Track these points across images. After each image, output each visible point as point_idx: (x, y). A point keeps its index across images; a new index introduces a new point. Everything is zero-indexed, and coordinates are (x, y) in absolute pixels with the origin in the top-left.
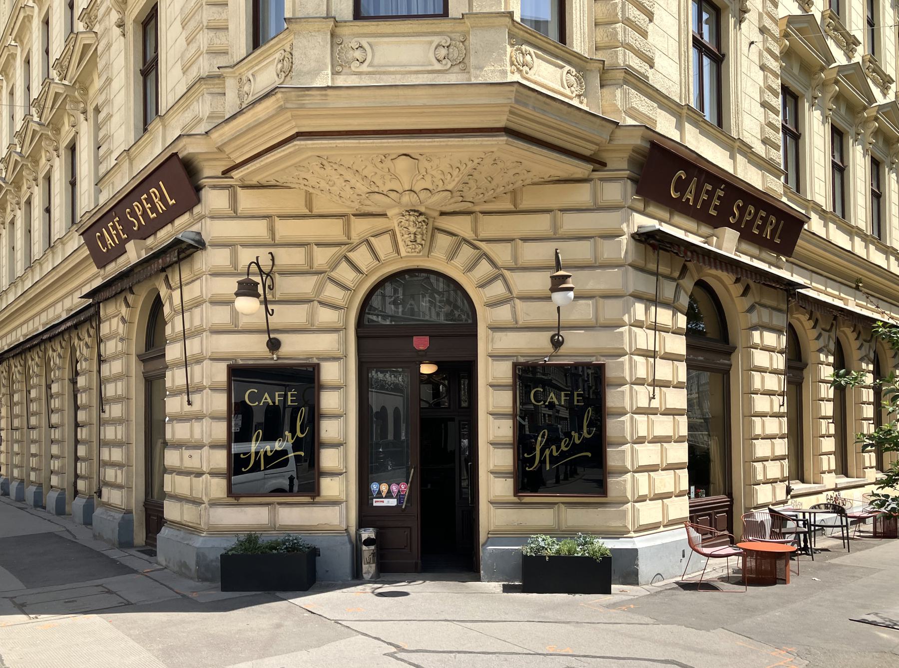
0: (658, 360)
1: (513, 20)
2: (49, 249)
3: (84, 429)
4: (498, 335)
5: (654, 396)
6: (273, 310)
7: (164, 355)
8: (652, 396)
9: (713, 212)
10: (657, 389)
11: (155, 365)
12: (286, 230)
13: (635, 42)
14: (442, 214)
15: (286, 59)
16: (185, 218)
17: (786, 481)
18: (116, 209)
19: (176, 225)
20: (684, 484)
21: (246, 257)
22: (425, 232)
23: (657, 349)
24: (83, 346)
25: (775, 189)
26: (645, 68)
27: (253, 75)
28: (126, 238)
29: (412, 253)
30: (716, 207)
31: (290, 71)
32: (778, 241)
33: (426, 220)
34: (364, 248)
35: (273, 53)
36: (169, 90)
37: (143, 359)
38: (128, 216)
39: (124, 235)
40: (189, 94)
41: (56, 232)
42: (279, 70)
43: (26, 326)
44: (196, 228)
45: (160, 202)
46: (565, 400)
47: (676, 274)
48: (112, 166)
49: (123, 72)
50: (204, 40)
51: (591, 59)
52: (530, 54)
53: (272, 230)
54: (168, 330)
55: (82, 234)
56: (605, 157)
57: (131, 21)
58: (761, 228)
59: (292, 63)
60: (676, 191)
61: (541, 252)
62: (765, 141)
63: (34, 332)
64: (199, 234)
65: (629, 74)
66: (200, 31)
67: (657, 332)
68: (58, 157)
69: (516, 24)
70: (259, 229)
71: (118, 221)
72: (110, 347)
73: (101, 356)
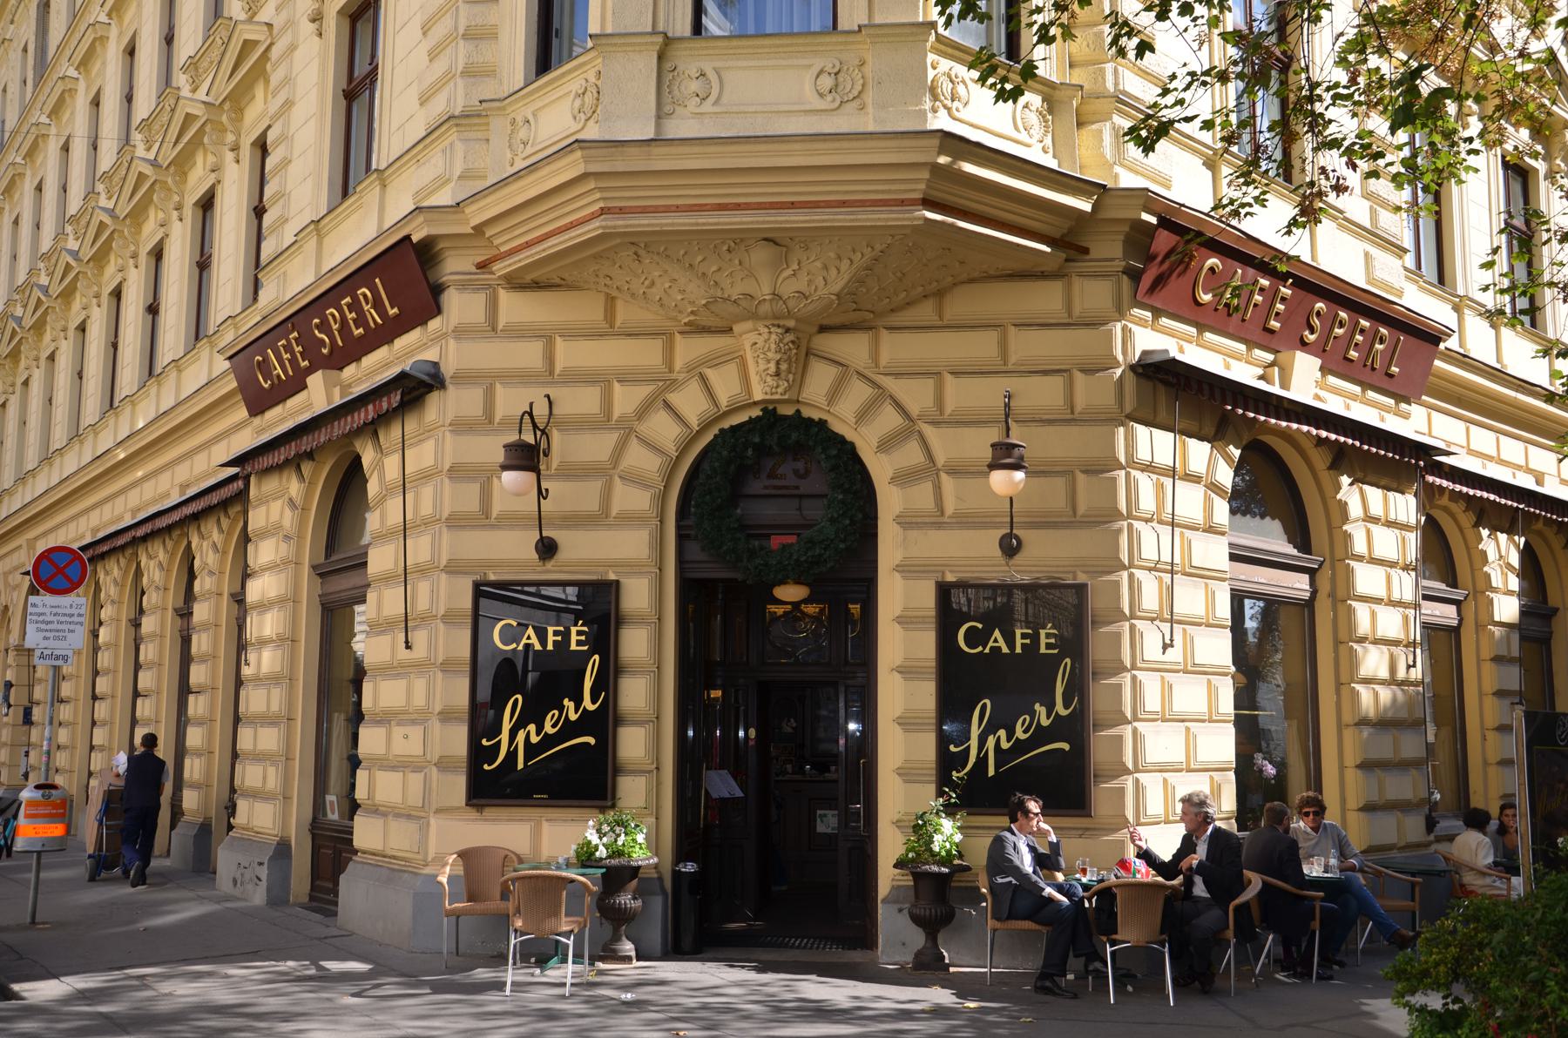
4: (913, 534)
6: (547, 490)
7: (365, 563)
8: (1168, 641)
12: (569, 354)
14: (823, 329)
15: (588, 93)
16: (413, 337)
18: (293, 320)
19: (395, 348)
21: (511, 403)
23: (1177, 560)
24: (208, 547)
27: (534, 115)
28: (308, 368)
29: (772, 394)
31: (594, 112)
34: (694, 387)
35: (570, 79)
36: (393, 128)
37: (323, 573)
38: (316, 332)
41: (166, 349)
42: (576, 111)
44: (431, 355)
45: (372, 311)
48: (284, 247)
49: (315, 90)
50: (461, 53)
52: (964, 82)
53: (550, 358)
54: (373, 521)
55: (230, 358)
57: (334, 14)
59: (598, 100)
61: (985, 394)
63: (113, 523)
64: (436, 365)
66: (450, 43)
68: (181, 220)
70: (529, 355)
71: (296, 339)
72: (264, 553)
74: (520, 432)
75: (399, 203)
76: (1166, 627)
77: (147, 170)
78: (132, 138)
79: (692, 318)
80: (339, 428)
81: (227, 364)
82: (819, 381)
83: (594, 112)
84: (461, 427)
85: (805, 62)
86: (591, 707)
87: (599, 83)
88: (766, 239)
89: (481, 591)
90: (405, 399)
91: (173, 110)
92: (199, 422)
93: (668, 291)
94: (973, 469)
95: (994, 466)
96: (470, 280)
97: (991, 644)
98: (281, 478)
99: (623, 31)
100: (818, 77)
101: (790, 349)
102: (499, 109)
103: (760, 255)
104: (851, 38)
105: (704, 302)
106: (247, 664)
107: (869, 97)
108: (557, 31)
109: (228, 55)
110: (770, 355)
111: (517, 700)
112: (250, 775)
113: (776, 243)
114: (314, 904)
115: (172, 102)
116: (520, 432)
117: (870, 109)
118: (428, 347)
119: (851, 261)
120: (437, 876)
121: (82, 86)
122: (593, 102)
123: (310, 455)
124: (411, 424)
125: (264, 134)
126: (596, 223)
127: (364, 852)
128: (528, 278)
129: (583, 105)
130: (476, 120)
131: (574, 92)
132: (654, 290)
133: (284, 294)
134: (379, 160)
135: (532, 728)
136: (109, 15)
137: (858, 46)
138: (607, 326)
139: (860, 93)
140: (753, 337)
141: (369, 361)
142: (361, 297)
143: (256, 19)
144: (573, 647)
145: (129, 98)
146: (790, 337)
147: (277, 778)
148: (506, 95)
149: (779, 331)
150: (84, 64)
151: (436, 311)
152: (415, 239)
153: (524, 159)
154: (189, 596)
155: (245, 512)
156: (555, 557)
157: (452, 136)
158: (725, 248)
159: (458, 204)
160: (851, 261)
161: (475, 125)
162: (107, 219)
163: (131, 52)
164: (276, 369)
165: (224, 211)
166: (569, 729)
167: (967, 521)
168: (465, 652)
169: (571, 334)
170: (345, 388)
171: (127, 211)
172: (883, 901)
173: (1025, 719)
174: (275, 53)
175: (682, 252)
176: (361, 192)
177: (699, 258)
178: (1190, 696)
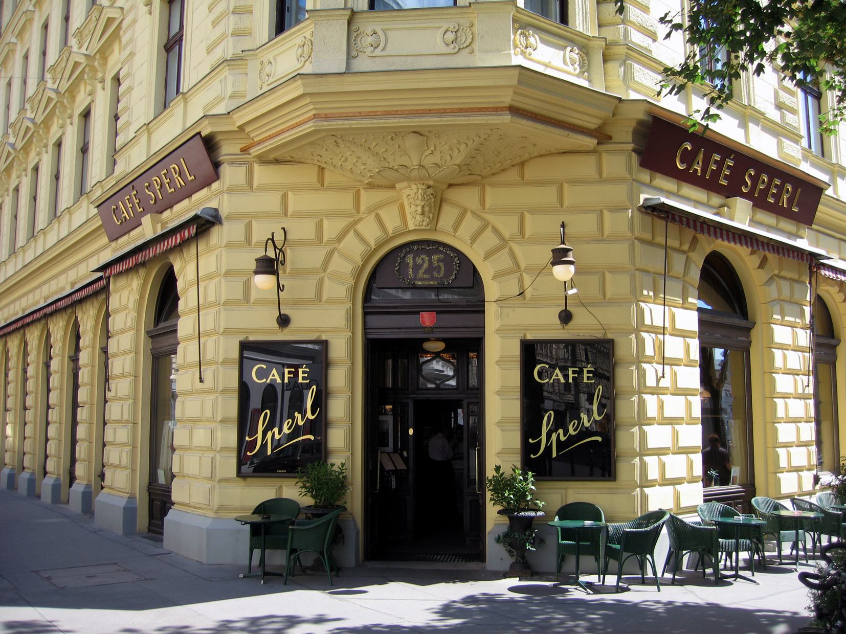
0: (667, 337)
1: (517, 7)
2: (56, 219)
3: (54, 411)
5: (663, 374)
6: (283, 286)
7: (176, 330)
9: (724, 183)
10: (667, 368)
11: (165, 342)
13: (636, 19)
14: (450, 186)
16: (204, 192)
17: (813, 470)
20: (698, 470)
21: (261, 232)
22: (433, 205)
24: (88, 318)
25: (792, 155)
26: (648, 42)
27: (274, 59)
30: (726, 177)
31: (309, 57)
33: (435, 194)
35: (296, 36)
37: (152, 336)
40: (212, 74)
43: (25, 298)
44: (214, 204)
45: (179, 178)
46: (573, 378)
47: (686, 247)
50: (231, 23)
51: (593, 37)
55: (98, 207)
56: (610, 130)
58: (778, 197)
59: (312, 49)
60: (682, 162)
62: (780, 106)
64: (216, 210)
65: (631, 50)
66: (226, 16)
67: (666, 308)
68: (72, 124)
69: (520, 10)
73: (109, 332)
74: (266, 251)
75: (195, 114)
76: (660, 368)
77: (53, 95)
78: (45, 77)
79: (370, 180)
80: (160, 248)
81: (96, 211)
82: (448, 216)
83: (309, 57)
84: (230, 246)
85: (437, 25)
86: (311, 417)
87: (312, 39)
88: (415, 132)
89: (245, 346)
90: (199, 231)
91: (67, 60)
92: (76, 248)
93: (356, 164)
95: (555, 263)
96: (237, 159)
98: (127, 278)
99: (327, 8)
100: (445, 34)
101: (430, 199)
102: (254, 55)
103: (411, 141)
104: (465, 10)
105: (377, 170)
106: (109, 390)
107: (476, 46)
108: (288, 7)
109: (99, 26)
110: (418, 202)
111: (266, 413)
112: (113, 455)
113: (421, 135)
114: (151, 534)
115: (68, 55)
116: (266, 251)
117: (477, 53)
118: (211, 200)
119: (467, 145)
120: (598, 144)
121: (19, 47)
122: (309, 50)
123: (143, 264)
124: (202, 245)
125: (118, 73)
126: (311, 124)
127: (178, 504)
128: (272, 157)
129: (303, 53)
130: (240, 62)
131: (297, 45)
132: (347, 163)
133: (129, 168)
134: (184, 88)
136: (34, 6)
137: (469, 15)
138: (319, 185)
139: (470, 43)
140: (407, 191)
141: (177, 208)
142: (173, 170)
143: (116, 5)
144: (300, 381)
145: (44, 53)
146: (430, 191)
147: (127, 459)
148: (258, 46)
149: (423, 187)
150: (20, 35)
151: (216, 178)
152: (203, 134)
153: (268, 85)
154: (77, 349)
155: (108, 298)
156: (289, 326)
157: (225, 72)
158: (390, 137)
159: (229, 113)
160: (467, 145)
161: (239, 65)
162: (30, 125)
163: (46, 27)
164: (123, 213)
165: (96, 118)
167: (539, 302)
168: (235, 383)
169: (296, 189)
170: (164, 224)
171: (41, 120)
172: (489, 533)
173: (575, 423)
174: (125, 25)
175: (363, 141)
176: (173, 106)
177: (374, 144)
178: (675, 406)
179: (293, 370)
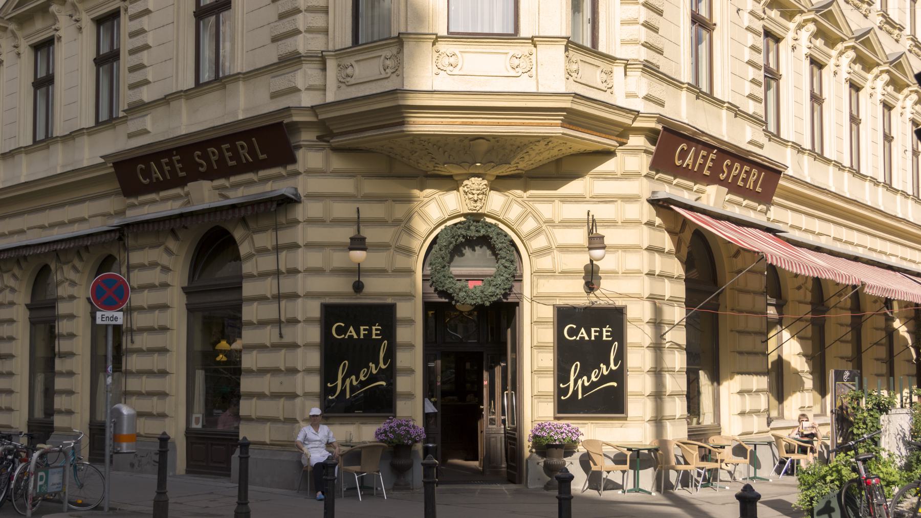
32: (262, 157)
39: (760, 187)
60: (145, 179)
94: (341, 248)
97: (580, 335)
111: (345, 364)
135: (585, 378)
144: (604, 338)
166: (604, 379)
179: (367, 327)
